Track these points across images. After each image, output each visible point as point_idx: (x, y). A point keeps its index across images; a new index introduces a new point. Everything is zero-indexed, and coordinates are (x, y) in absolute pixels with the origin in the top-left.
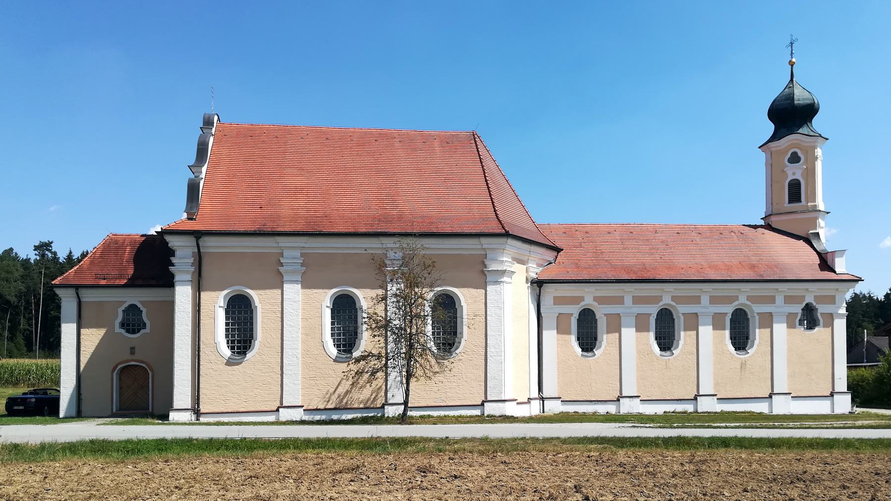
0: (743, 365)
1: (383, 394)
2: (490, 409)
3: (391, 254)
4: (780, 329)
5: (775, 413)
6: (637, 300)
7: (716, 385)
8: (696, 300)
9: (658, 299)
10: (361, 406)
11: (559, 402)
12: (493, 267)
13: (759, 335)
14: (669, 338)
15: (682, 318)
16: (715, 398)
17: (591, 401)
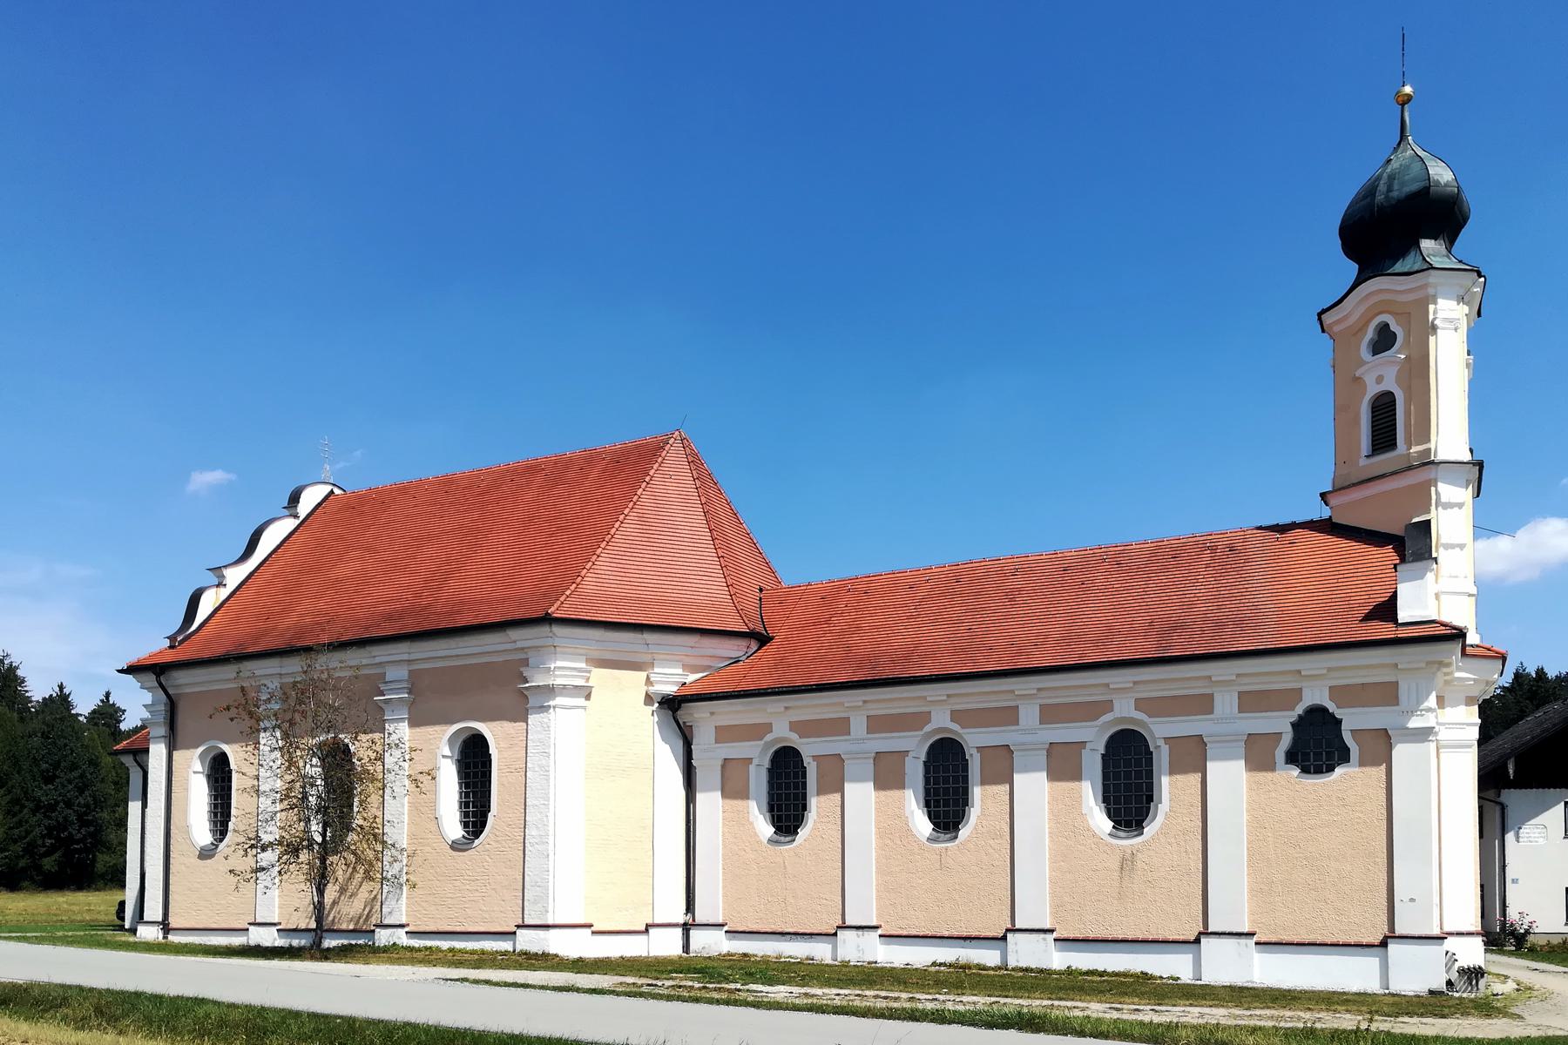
0: (1127, 863)
1: (378, 907)
2: (528, 941)
3: (392, 673)
4: (1228, 776)
5: (1206, 980)
6: (877, 724)
7: (1058, 908)
8: (1009, 716)
9: (921, 719)
10: (351, 927)
11: (720, 934)
12: (538, 680)
13: (1171, 789)
14: (956, 803)
15: (1165, 749)
16: (1050, 937)
17: (782, 934)
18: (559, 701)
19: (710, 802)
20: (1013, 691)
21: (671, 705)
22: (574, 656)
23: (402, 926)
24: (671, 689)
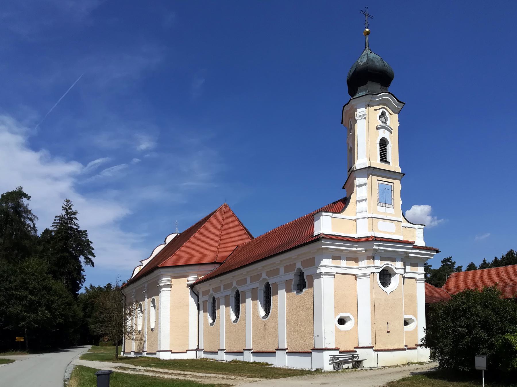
18: (163, 289)
19: (202, 312)
20: (242, 274)
21: (192, 287)
22: (167, 276)
23: (223, 350)
24: (192, 282)
